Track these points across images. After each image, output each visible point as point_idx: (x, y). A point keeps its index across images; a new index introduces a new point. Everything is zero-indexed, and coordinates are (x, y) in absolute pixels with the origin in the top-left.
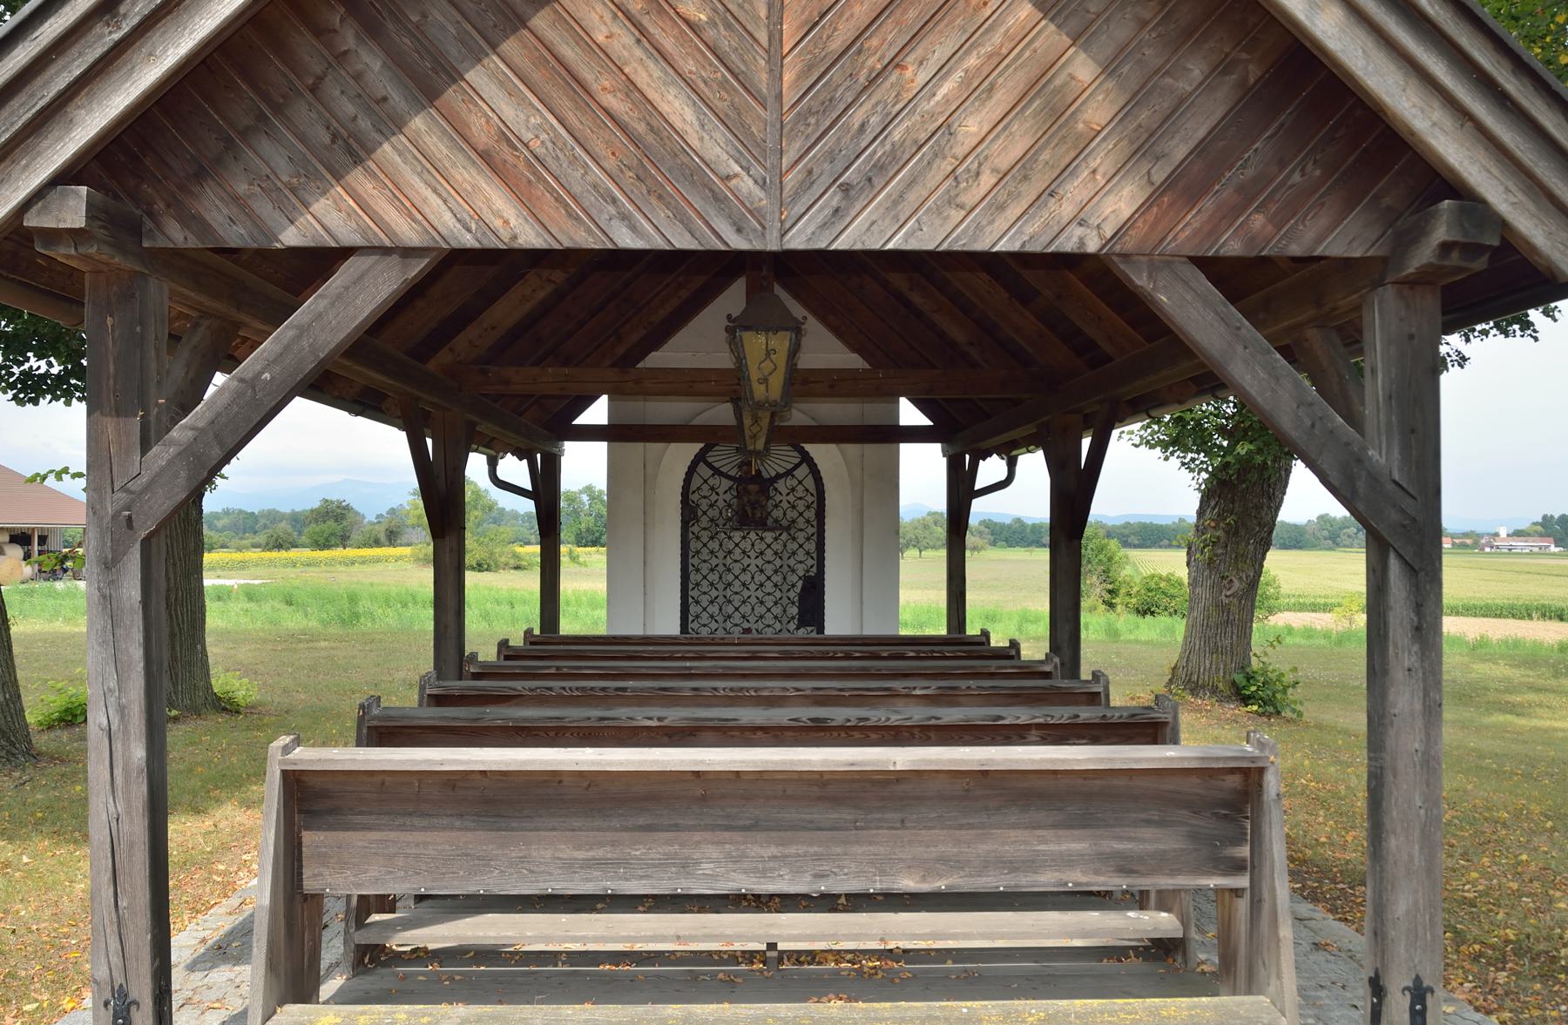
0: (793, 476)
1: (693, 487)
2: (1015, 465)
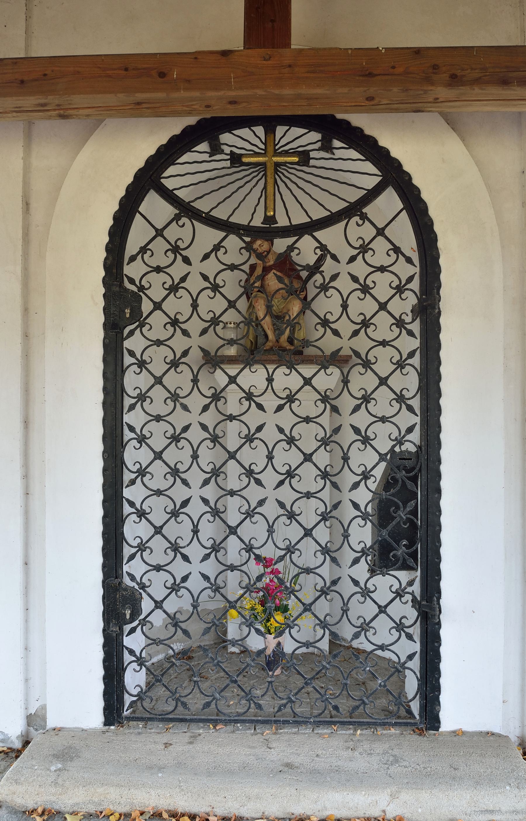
0: (364, 217)
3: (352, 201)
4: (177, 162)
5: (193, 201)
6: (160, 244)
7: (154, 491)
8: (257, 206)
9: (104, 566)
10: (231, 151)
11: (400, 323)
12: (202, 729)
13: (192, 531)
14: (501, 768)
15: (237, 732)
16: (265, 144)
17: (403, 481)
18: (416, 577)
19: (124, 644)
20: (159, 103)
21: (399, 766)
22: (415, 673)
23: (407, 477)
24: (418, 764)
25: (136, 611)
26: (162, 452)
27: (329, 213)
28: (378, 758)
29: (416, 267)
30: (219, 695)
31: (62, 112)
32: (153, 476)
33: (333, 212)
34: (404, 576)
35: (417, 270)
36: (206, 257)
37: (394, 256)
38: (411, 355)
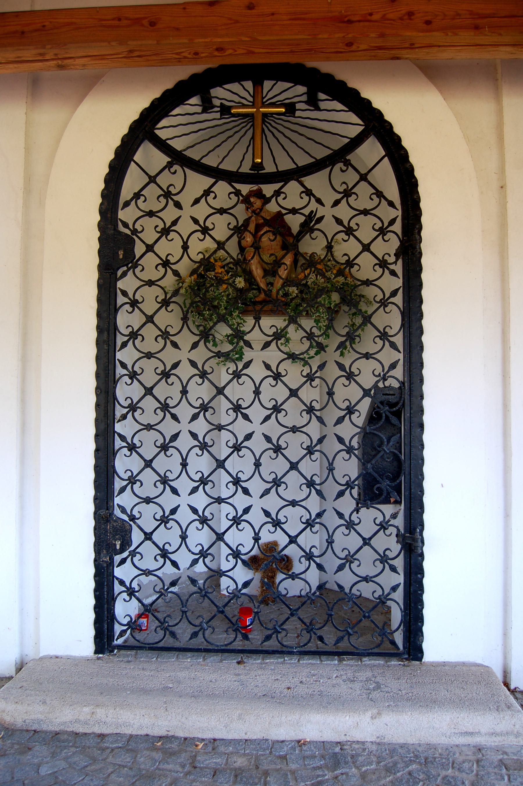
0: (348, 163)
1: (126, 193)
2: (196, 204)
3: (336, 148)
4: (170, 114)
5: (184, 150)
6: (152, 191)
7: (144, 425)
8: (245, 154)
9: (96, 499)
10: (221, 103)
11: (383, 264)
12: (190, 659)
13: (181, 464)
14: (481, 693)
15: (224, 661)
16: (253, 97)
17: (387, 416)
18: (400, 510)
19: (115, 574)
20: (150, 51)
21: (381, 691)
22: (398, 604)
23: (390, 412)
24: (400, 690)
25: (126, 543)
26: (152, 388)
27: (314, 160)
28: (361, 684)
29: (398, 210)
30: (206, 625)
31: (60, 62)
32: (143, 411)
33: (318, 159)
34: (388, 509)
35: (399, 213)
36: (197, 201)
37: (376, 200)
38: (394, 293)
